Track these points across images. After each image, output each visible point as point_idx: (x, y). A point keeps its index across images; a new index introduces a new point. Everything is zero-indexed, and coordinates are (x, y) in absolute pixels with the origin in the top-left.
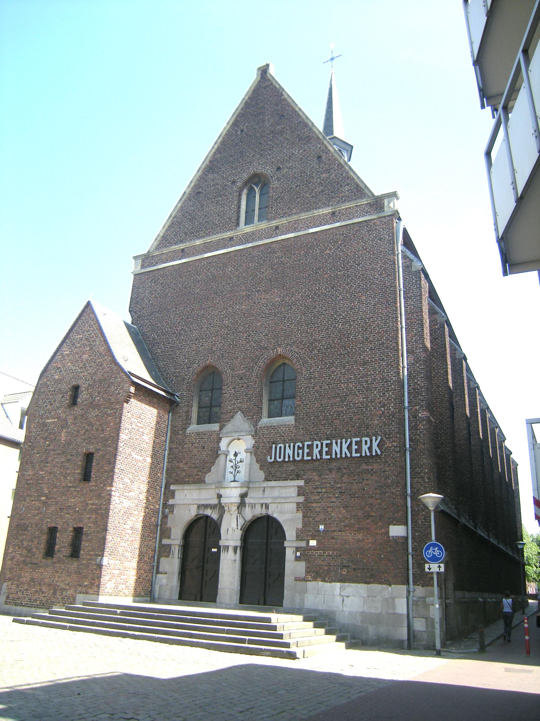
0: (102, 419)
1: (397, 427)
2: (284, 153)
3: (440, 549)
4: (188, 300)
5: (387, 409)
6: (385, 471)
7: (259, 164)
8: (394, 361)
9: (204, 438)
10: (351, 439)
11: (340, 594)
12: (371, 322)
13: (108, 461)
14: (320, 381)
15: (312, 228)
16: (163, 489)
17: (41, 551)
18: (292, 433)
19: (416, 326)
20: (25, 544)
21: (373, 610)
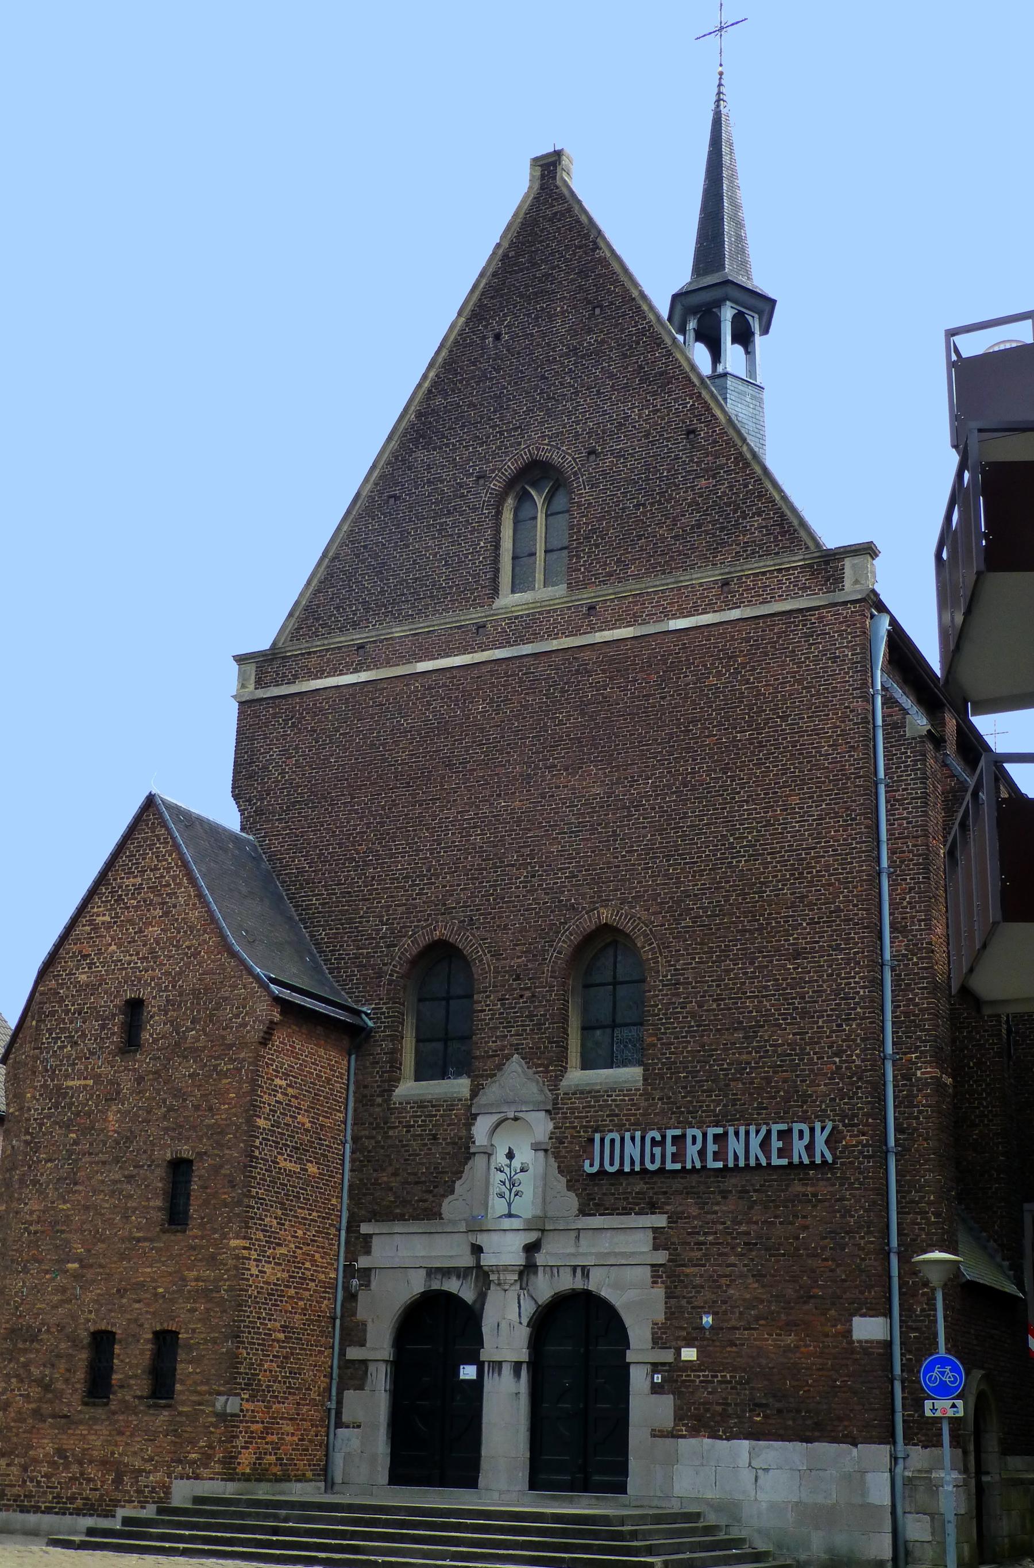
0: (207, 1082)
1: (869, 1103)
2: (605, 412)
3: (955, 1369)
4: (380, 777)
5: (846, 1061)
6: (842, 1199)
7: (543, 437)
8: (863, 952)
9: (436, 1116)
10: (767, 1124)
11: (750, 1465)
12: (813, 858)
13: (230, 1182)
14: (700, 992)
15: (674, 617)
16: (343, 1233)
17: (78, 1386)
18: (639, 1109)
19: (913, 869)
20: (36, 1372)
21: (820, 1499)
